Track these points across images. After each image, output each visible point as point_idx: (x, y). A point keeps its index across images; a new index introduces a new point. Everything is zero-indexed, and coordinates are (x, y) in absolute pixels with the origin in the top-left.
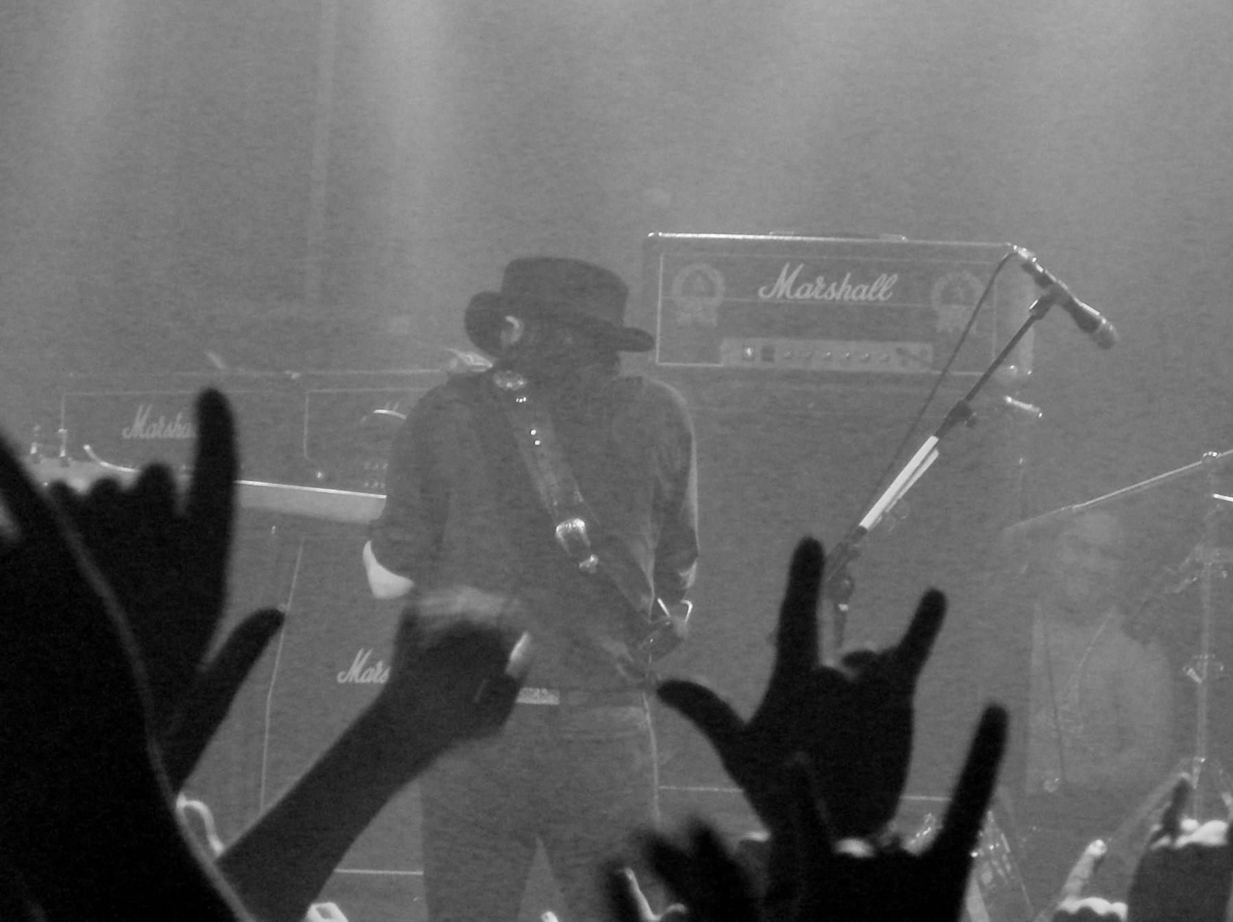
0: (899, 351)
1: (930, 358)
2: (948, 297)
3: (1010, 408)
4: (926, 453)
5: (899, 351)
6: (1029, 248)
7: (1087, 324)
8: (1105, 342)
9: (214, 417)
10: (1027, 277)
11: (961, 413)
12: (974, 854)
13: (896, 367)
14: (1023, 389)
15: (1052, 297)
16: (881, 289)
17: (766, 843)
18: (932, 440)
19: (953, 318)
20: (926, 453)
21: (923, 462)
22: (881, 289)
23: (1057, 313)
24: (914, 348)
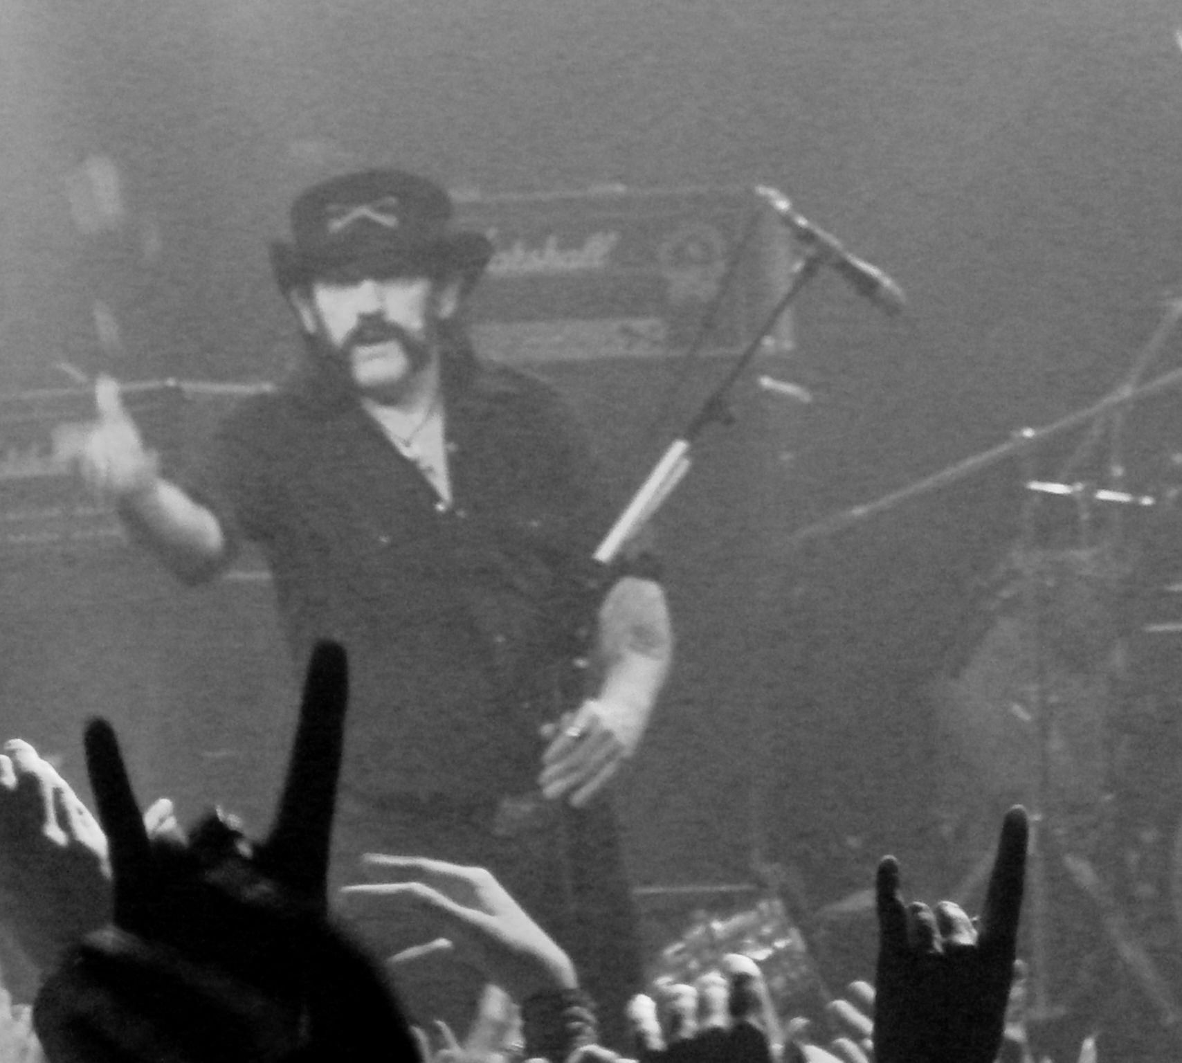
0: (626, 331)
1: (660, 335)
2: (680, 257)
3: (768, 394)
4: (674, 461)
5: (626, 331)
6: (788, 192)
7: (867, 286)
8: (891, 309)
9: (887, 880)
10: (783, 231)
11: (715, 409)
12: (81, 959)
13: (619, 349)
14: (785, 368)
15: (820, 261)
16: (595, 253)
17: (658, 975)
18: (679, 448)
19: (691, 284)
20: (674, 461)
21: (671, 472)
22: (595, 253)
23: (825, 272)
24: (641, 325)
